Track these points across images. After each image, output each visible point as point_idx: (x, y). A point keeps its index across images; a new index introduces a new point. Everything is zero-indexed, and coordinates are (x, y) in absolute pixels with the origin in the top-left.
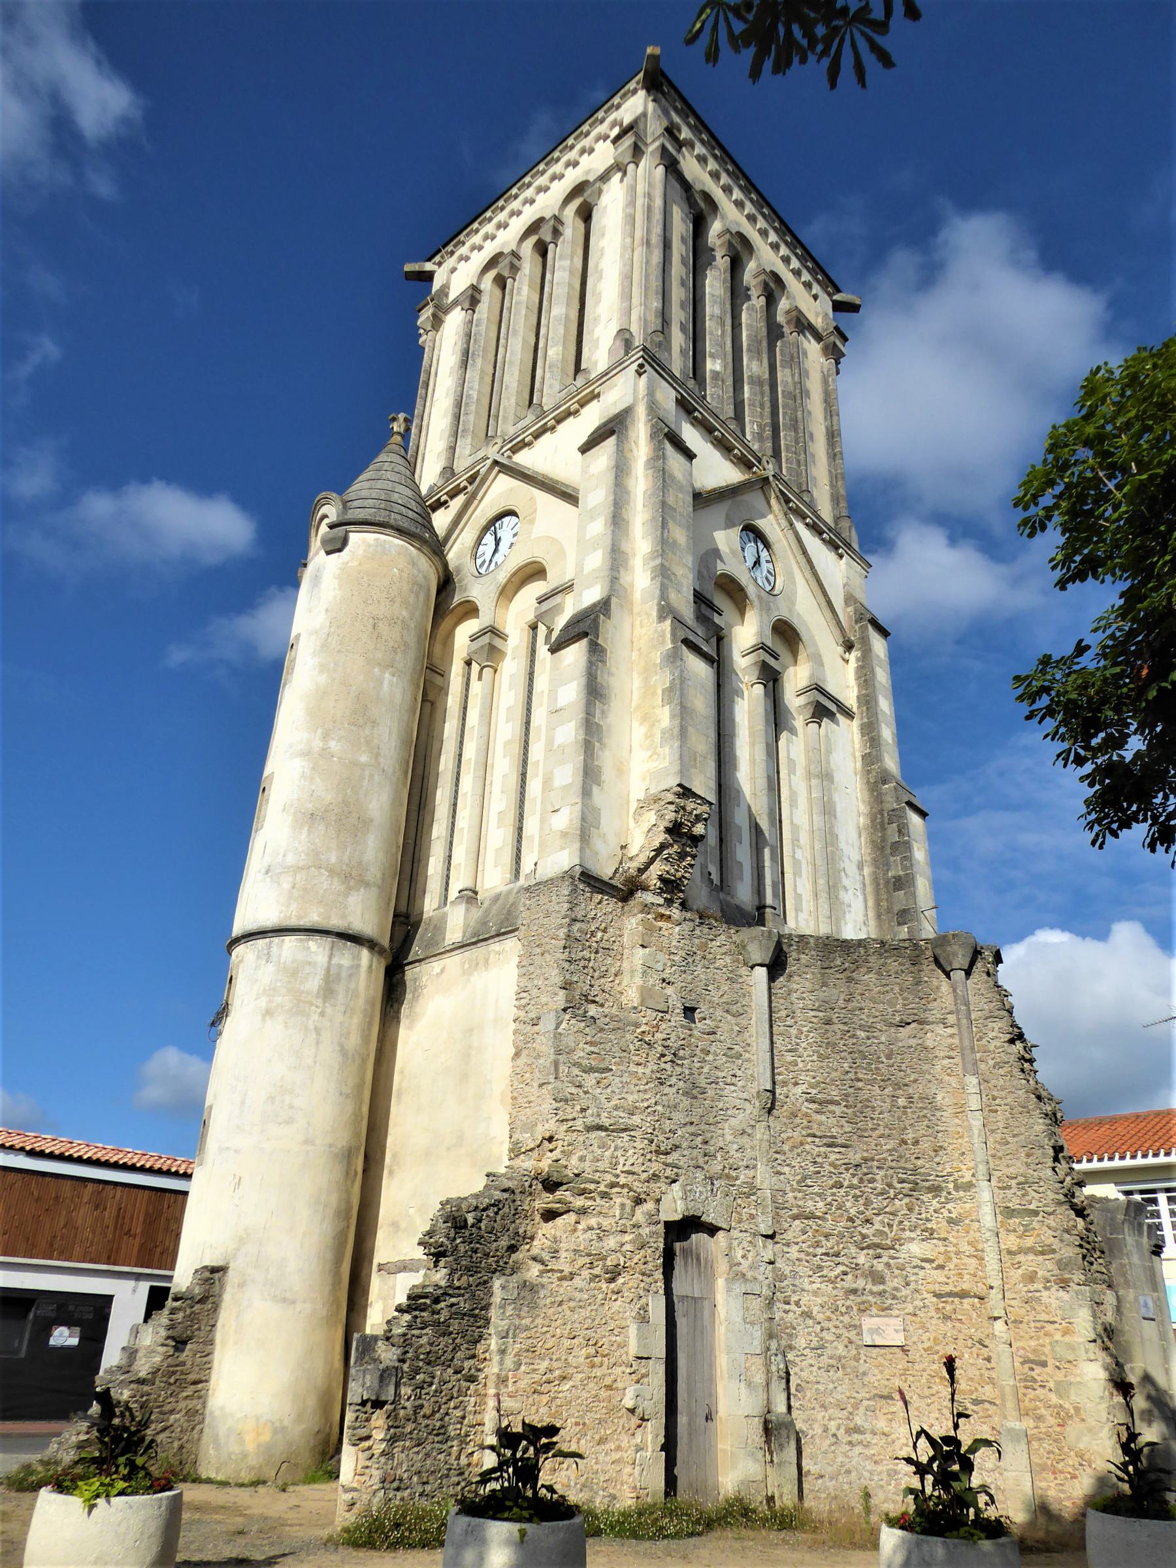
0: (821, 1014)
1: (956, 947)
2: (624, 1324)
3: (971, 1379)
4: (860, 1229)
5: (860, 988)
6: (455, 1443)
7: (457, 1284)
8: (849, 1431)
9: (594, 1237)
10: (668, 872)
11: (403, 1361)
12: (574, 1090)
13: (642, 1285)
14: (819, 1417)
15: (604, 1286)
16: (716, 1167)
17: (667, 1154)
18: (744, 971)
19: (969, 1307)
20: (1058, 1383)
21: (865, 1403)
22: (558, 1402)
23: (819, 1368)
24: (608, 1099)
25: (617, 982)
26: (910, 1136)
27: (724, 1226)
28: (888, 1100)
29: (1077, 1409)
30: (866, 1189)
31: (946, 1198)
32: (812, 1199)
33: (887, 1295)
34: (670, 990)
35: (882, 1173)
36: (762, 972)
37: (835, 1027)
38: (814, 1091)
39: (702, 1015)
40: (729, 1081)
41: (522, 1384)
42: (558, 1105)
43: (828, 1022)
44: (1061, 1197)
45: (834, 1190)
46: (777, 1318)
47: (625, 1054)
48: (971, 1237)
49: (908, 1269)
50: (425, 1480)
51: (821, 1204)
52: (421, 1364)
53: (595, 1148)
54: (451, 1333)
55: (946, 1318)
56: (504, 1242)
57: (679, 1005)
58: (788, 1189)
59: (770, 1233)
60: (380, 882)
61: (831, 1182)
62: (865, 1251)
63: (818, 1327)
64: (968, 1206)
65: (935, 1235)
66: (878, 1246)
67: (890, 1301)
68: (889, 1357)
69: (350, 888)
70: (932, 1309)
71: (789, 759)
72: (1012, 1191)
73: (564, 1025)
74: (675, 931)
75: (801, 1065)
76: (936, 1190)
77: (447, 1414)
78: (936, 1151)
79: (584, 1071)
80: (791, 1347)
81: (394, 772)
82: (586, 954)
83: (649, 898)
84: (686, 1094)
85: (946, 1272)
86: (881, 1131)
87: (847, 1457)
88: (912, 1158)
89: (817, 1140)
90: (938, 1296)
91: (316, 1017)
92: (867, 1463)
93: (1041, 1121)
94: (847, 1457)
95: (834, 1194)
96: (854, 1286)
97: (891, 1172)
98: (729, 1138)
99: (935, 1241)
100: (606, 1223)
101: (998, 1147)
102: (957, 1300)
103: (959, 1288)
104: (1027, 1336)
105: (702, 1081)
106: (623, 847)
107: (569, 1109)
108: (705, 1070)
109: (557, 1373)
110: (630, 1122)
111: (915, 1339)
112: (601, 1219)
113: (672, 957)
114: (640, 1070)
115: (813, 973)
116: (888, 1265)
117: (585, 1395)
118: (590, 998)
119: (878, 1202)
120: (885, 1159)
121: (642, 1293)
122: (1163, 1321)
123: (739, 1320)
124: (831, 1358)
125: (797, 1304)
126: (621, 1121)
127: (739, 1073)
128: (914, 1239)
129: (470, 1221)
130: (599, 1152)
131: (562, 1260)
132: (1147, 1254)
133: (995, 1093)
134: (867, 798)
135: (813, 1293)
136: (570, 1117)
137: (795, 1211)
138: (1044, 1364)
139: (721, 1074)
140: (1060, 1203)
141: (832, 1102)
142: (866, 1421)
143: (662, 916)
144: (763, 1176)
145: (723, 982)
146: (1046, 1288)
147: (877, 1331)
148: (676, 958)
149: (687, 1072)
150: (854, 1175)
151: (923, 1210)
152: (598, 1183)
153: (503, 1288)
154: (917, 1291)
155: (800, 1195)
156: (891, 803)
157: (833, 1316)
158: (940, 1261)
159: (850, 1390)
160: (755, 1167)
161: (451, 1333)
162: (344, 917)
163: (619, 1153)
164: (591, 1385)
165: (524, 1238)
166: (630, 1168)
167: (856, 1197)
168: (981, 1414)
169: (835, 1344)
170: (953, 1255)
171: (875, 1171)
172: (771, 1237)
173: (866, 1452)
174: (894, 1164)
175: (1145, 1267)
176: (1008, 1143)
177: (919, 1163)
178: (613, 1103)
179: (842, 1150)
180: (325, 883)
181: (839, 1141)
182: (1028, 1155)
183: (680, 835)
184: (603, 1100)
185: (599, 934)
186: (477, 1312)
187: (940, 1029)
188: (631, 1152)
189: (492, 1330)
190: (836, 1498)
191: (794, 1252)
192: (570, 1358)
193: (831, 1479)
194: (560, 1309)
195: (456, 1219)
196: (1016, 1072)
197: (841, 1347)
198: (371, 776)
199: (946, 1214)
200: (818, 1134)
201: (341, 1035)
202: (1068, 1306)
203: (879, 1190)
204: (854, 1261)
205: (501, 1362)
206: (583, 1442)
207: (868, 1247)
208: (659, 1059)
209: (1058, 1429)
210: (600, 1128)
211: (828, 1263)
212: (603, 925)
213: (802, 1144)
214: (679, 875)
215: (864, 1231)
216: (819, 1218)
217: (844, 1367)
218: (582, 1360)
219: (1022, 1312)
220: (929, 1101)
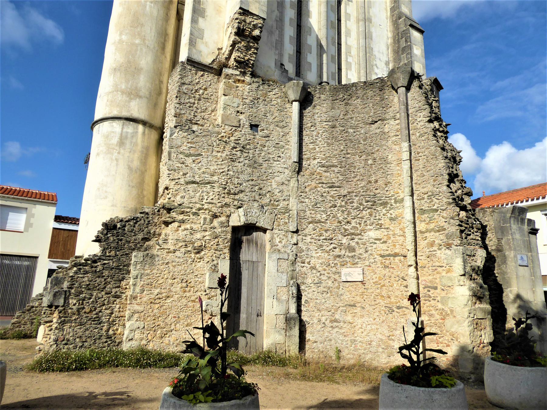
0: (330, 123)
1: (399, 74)
2: (203, 273)
3: (397, 297)
4: (344, 226)
5: (352, 108)
6: (106, 324)
7: (108, 254)
8: (331, 321)
9: (188, 233)
10: (239, 57)
11: (71, 288)
12: (180, 165)
13: (215, 255)
14: (317, 315)
15: (193, 255)
16: (266, 200)
17: (235, 194)
18: (288, 105)
19: (398, 261)
20: (442, 298)
21: (341, 308)
22: (165, 307)
23: (318, 292)
24: (199, 169)
25: (213, 114)
26: (373, 179)
27: (269, 228)
28: (363, 162)
29: (452, 311)
30: (349, 207)
31: (390, 207)
32: (319, 213)
33: (356, 257)
34: (242, 117)
35: (357, 198)
36: (296, 105)
37: (337, 129)
38: (324, 162)
39: (261, 128)
40: (276, 159)
41: (145, 299)
42: (170, 172)
43: (334, 127)
44: (451, 201)
45: (332, 209)
46: (297, 270)
47: (211, 147)
48: (401, 226)
49: (368, 244)
50: (84, 340)
51: (324, 216)
52: (83, 290)
53: (191, 192)
54: (104, 276)
55: (386, 267)
56: (140, 236)
57: (247, 124)
58: (307, 209)
59: (295, 230)
60: (148, 96)
61: (330, 205)
62: (346, 237)
63: (319, 273)
64: (400, 211)
65: (383, 227)
66: (353, 234)
67: (357, 260)
68: (355, 286)
69: (131, 99)
70: (379, 263)
71: (346, 12)
72: (425, 200)
73: (176, 134)
74: (247, 87)
75: (317, 149)
76: (385, 204)
77: (100, 312)
78: (386, 185)
79: (185, 156)
80: (303, 283)
81: (154, 47)
82: (192, 100)
83: (230, 71)
84: (249, 166)
85: (387, 244)
86: (358, 177)
87: (330, 333)
88: (374, 189)
89: (324, 185)
90: (382, 256)
91: (116, 154)
92: (340, 336)
93: (442, 161)
94: (330, 333)
95: (332, 211)
96: (340, 254)
97: (362, 197)
98: (274, 186)
99: (382, 230)
100: (195, 227)
101: (419, 178)
102: (392, 258)
103: (393, 252)
104: (427, 274)
105: (261, 160)
106: (219, 49)
107: (176, 174)
108: (263, 155)
109: (164, 295)
110: (212, 179)
111: (369, 278)
112: (192, 225)
113: (244, 100)
114: (219, 154)
115: (327, 104)
116: (357, 243)
117: (179, 304)
118: (194, 122)
119: (354, 213)
120: (359, 192)
121: (214, 259)
122: (533, 267)
123: (275, 271)
124: (324, 288)
125: (309, 263)
126: (206, 179)
127: (282, 155)
128: (371, 229)
129: (119, 225)
130: (193, 194)
131: (170, 244)
132: (526, 234)
133: (419, 150)
134: (392, 29)
135: (317, 257)
136: (177, 178)
137: (310, 220)
138: (436, 288)
139: (271, 156)
140: (450, 204)
141: (333, 166)
142: (341, 317)
143: (239, 80)
144: (293, 204)
145: (275, 111)
146: (439, 249)
147: (349, 274)
148: (247, 101)
149: (251, 156)
150: (342, 201)
151: (377, 215)
152: (192, 208)
153: (135, 256)
154: (371, 254)
155: (313, 212)
156: (403, 28)
157: (327, 268)
158: (385, 239)
159: (333, 302)
160: (288, 200)
161: (104, 276)
162: (129, 111)
163: (204, 194)
164: (183, 300)
165: (154, 235)
166: (211, 201)
167: (343, 212)
168: (401, 313)
169: (328, 281)
170: (391, 236)
171: (354, 198)
172: (297, 232)
173: (340, 331)
174: (364, 193)
175: (524, 241)
176: (424, 175)
177: (377, 191)
178: (202, 171)
179: (337, 189)
180: (120, 97)
181: (336, 185)
182: (434, 181)
183: (246, 37)
184: (196, 170)
185: (201, 91)
186: (121, 267)
187: (392, 122)
188: (211, 193)
189: (131, 276)
190: (322, 352)
191: (308, 239)
192: (172, 288)
193: (321, 343)
194: (167, 266)
195: (109, 227)
196: (431, 137)
197: (330, 282)
198: (141, 49)
199: (389, 215)
200: (325, 182)
201: (129, 161)
202: (450, 258)
203: (355, 207)
204: (340, 242)
205: (134, 290)
206: (178, 325)
207: (348, 235)
208: (232, 149)
209: (441, 321)
210: (194, 182)
211: (326, 244)
212: (204, 87)
213: (316, 187)
214: (246, 58)
215: (346, 227)
216: (323, 222)
217: (331, 292)
218: (178, 289)
219: (426, 262)
220: (385, 161)
